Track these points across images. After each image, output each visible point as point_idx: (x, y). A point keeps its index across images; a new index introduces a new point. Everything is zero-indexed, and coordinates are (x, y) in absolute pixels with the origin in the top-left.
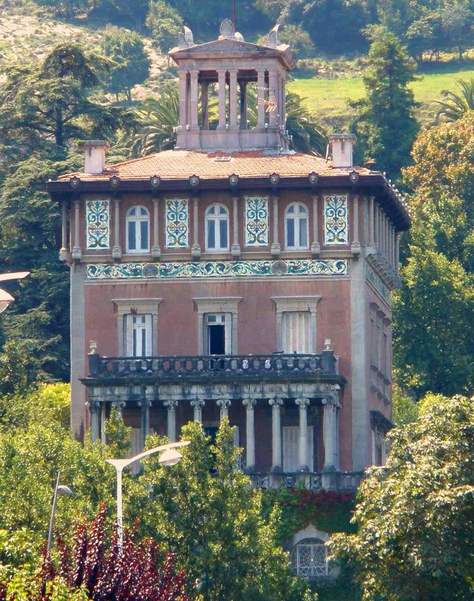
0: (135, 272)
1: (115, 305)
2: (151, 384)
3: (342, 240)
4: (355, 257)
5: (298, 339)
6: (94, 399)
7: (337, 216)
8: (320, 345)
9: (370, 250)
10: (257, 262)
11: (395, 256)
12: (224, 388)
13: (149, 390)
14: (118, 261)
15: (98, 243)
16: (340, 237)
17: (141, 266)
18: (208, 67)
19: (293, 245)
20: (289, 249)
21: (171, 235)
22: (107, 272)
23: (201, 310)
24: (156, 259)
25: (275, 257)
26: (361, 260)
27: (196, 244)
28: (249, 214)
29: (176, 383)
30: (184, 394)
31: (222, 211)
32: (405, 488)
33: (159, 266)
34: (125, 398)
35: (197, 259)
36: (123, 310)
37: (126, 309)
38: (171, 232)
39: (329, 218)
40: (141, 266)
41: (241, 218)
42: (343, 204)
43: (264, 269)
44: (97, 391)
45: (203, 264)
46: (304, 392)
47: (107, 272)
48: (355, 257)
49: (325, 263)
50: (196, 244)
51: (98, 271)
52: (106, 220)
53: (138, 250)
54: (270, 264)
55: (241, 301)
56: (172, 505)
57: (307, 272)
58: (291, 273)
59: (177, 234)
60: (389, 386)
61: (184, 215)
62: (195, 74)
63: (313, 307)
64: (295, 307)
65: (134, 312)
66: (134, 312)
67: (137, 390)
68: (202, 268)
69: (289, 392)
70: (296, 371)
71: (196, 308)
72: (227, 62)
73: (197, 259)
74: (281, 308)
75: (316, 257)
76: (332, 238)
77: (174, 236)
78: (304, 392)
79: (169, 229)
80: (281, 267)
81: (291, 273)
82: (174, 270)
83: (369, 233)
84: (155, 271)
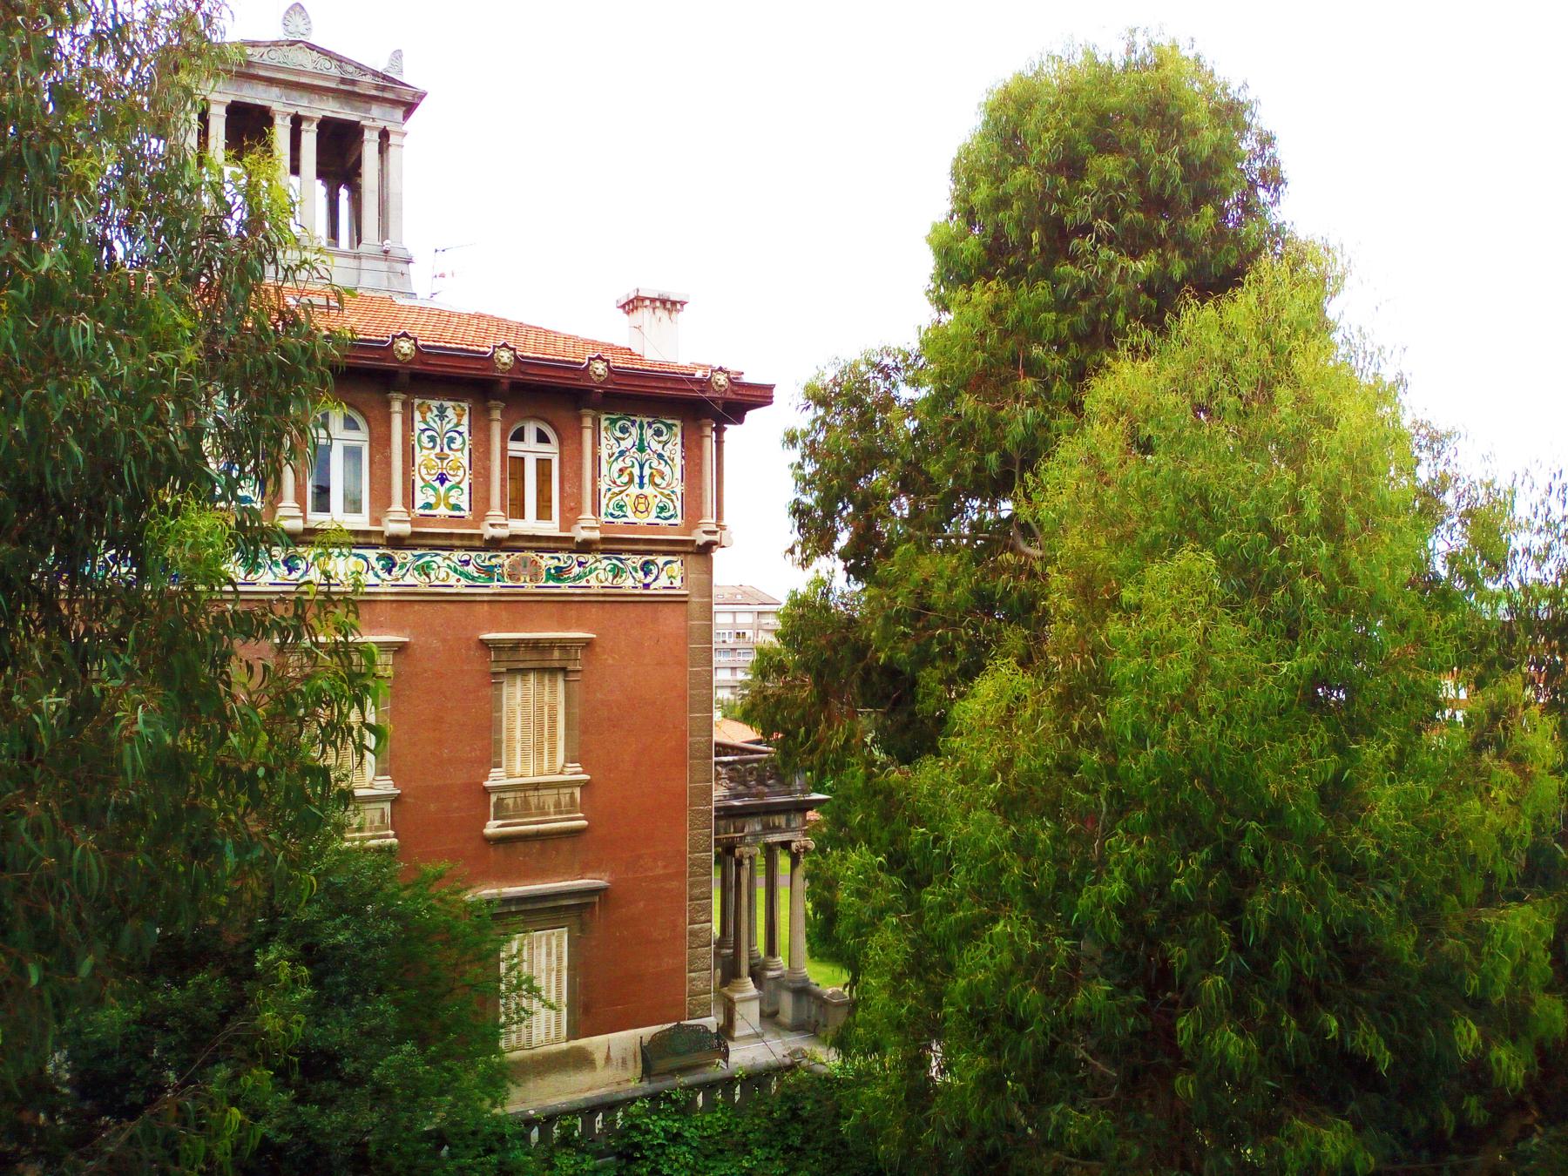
3: (456, 507)
6: (954, 947)
7: (446, 450)
10: (473, 554)
16: (452, 501)
19: (328, 510)
20: (316, 519)
21: (427, 484)
28: (424, 438)
32: (204, 1029)
38: (427, 478)
39: (425, 452)
42: (458, 425)
49: (620, 560)
51: (401, 568)
52: (462, 450)
57: (584, 583)
58: (551, 583)
59: (442, 483)
60: (1205, 972)
61: (459, 440)
68: (635, 570)
76: (432, 500)
77: (434, 489)
79: (423, 471)
81: (551, 583)
82: (576, 570)
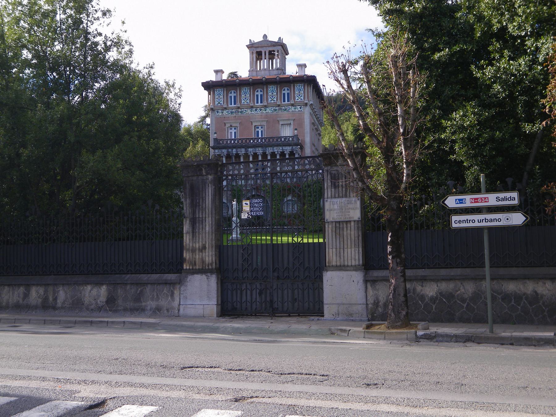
0: (232, 113)
1: (225, 124)
2: (235, 148)
4: (306, 105)
5: (287, 132)
8: (294, 133)
9: (311, 102)
11: (315, 342)
12: (260, 149)
13: (234, 150)
14: (226, 109)
15: (219, 103)
17: (234, 111)
18: (259, 50)
22: (222, 113)
23: (254, 125)
24: (239, 108)
25: (279, 106)
26: (308, 106)
27: (252, 102)
29: (243, 147)
30: (246, 151)
31: (261, 91)
33: (240, 110)
34: (225, 153)
35: (252, 107)
36: (228, 125)
37: (228, 125)
40: (234, 111)
41: (267, 93)
43: (275, 110)
44: (216, 151)
45: (254, 109)
46: (288, 149)
47: (222, 113)
48: (306, 105)
50: (252, 102)
53: (233, 105)
54: (277, 108)
55: (267, 121)
56: (535, 104)
62: (255, 52)
63: (292, 122)
64: (286, 122)
65: (231, 126)
66: (231, 126)
67: (230, 150)
69: (283, 149)
70: (286, 142)
71: (252, 124)
72: (265, 48)
73: (252, 107)
74: (281, 123)
75: (292, 105)
78: (288, 149)
80: (281, 109)
83: (311, 97)
84: (238, 112)
